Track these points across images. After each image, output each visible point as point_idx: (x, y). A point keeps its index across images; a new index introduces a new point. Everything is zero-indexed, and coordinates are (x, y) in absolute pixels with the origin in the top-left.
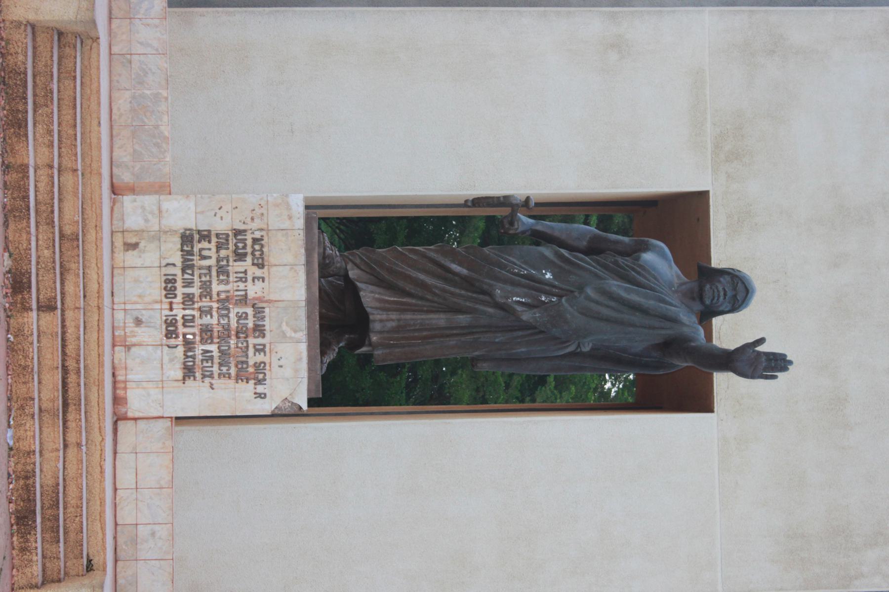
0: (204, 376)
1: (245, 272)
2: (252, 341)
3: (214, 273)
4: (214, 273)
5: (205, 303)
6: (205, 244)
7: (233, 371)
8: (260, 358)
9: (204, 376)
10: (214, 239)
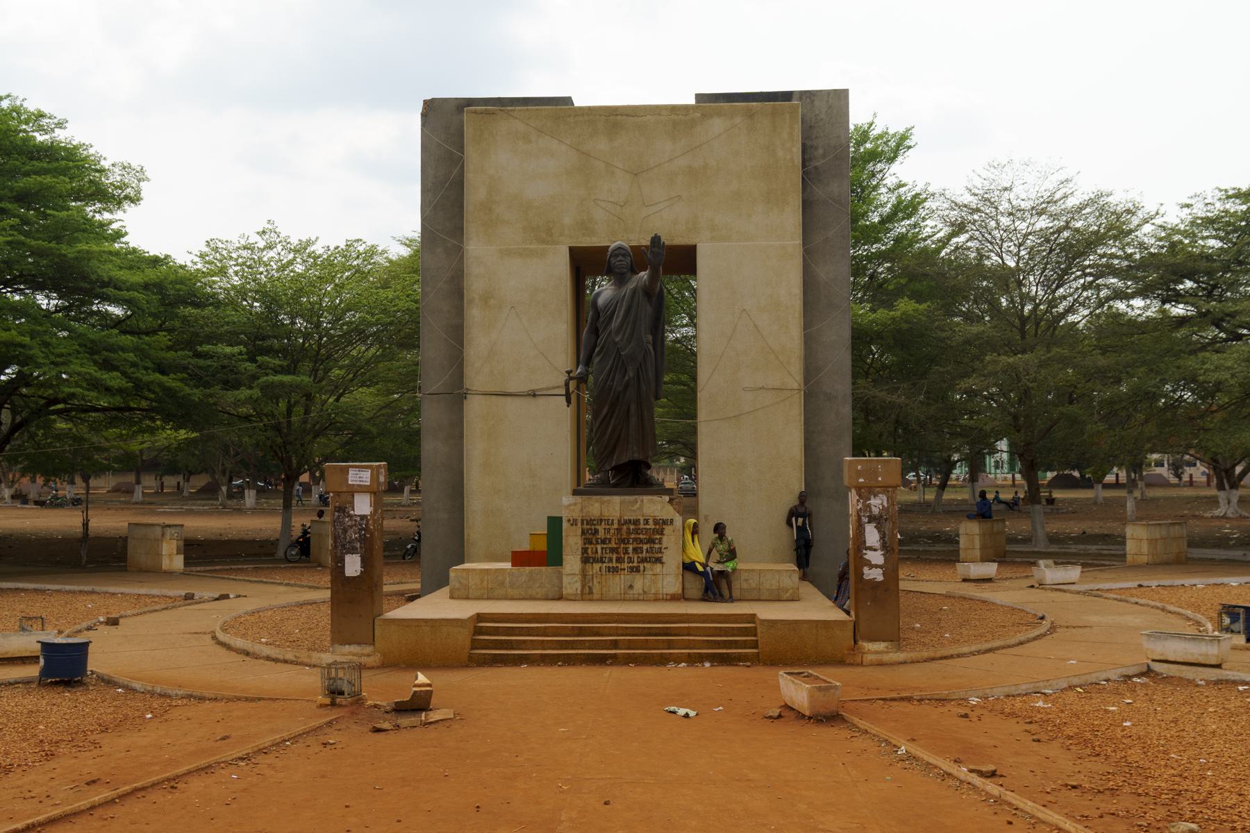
0: (661, 552)
1: (605, 529)
2: (642, 526)
3: (605, 546)
4: (605, 546)
5: (621, 550)
6: (590, 551)
7: (658, 537)
8: (651, 522)
9: (661, 552)
10: (587, 546)
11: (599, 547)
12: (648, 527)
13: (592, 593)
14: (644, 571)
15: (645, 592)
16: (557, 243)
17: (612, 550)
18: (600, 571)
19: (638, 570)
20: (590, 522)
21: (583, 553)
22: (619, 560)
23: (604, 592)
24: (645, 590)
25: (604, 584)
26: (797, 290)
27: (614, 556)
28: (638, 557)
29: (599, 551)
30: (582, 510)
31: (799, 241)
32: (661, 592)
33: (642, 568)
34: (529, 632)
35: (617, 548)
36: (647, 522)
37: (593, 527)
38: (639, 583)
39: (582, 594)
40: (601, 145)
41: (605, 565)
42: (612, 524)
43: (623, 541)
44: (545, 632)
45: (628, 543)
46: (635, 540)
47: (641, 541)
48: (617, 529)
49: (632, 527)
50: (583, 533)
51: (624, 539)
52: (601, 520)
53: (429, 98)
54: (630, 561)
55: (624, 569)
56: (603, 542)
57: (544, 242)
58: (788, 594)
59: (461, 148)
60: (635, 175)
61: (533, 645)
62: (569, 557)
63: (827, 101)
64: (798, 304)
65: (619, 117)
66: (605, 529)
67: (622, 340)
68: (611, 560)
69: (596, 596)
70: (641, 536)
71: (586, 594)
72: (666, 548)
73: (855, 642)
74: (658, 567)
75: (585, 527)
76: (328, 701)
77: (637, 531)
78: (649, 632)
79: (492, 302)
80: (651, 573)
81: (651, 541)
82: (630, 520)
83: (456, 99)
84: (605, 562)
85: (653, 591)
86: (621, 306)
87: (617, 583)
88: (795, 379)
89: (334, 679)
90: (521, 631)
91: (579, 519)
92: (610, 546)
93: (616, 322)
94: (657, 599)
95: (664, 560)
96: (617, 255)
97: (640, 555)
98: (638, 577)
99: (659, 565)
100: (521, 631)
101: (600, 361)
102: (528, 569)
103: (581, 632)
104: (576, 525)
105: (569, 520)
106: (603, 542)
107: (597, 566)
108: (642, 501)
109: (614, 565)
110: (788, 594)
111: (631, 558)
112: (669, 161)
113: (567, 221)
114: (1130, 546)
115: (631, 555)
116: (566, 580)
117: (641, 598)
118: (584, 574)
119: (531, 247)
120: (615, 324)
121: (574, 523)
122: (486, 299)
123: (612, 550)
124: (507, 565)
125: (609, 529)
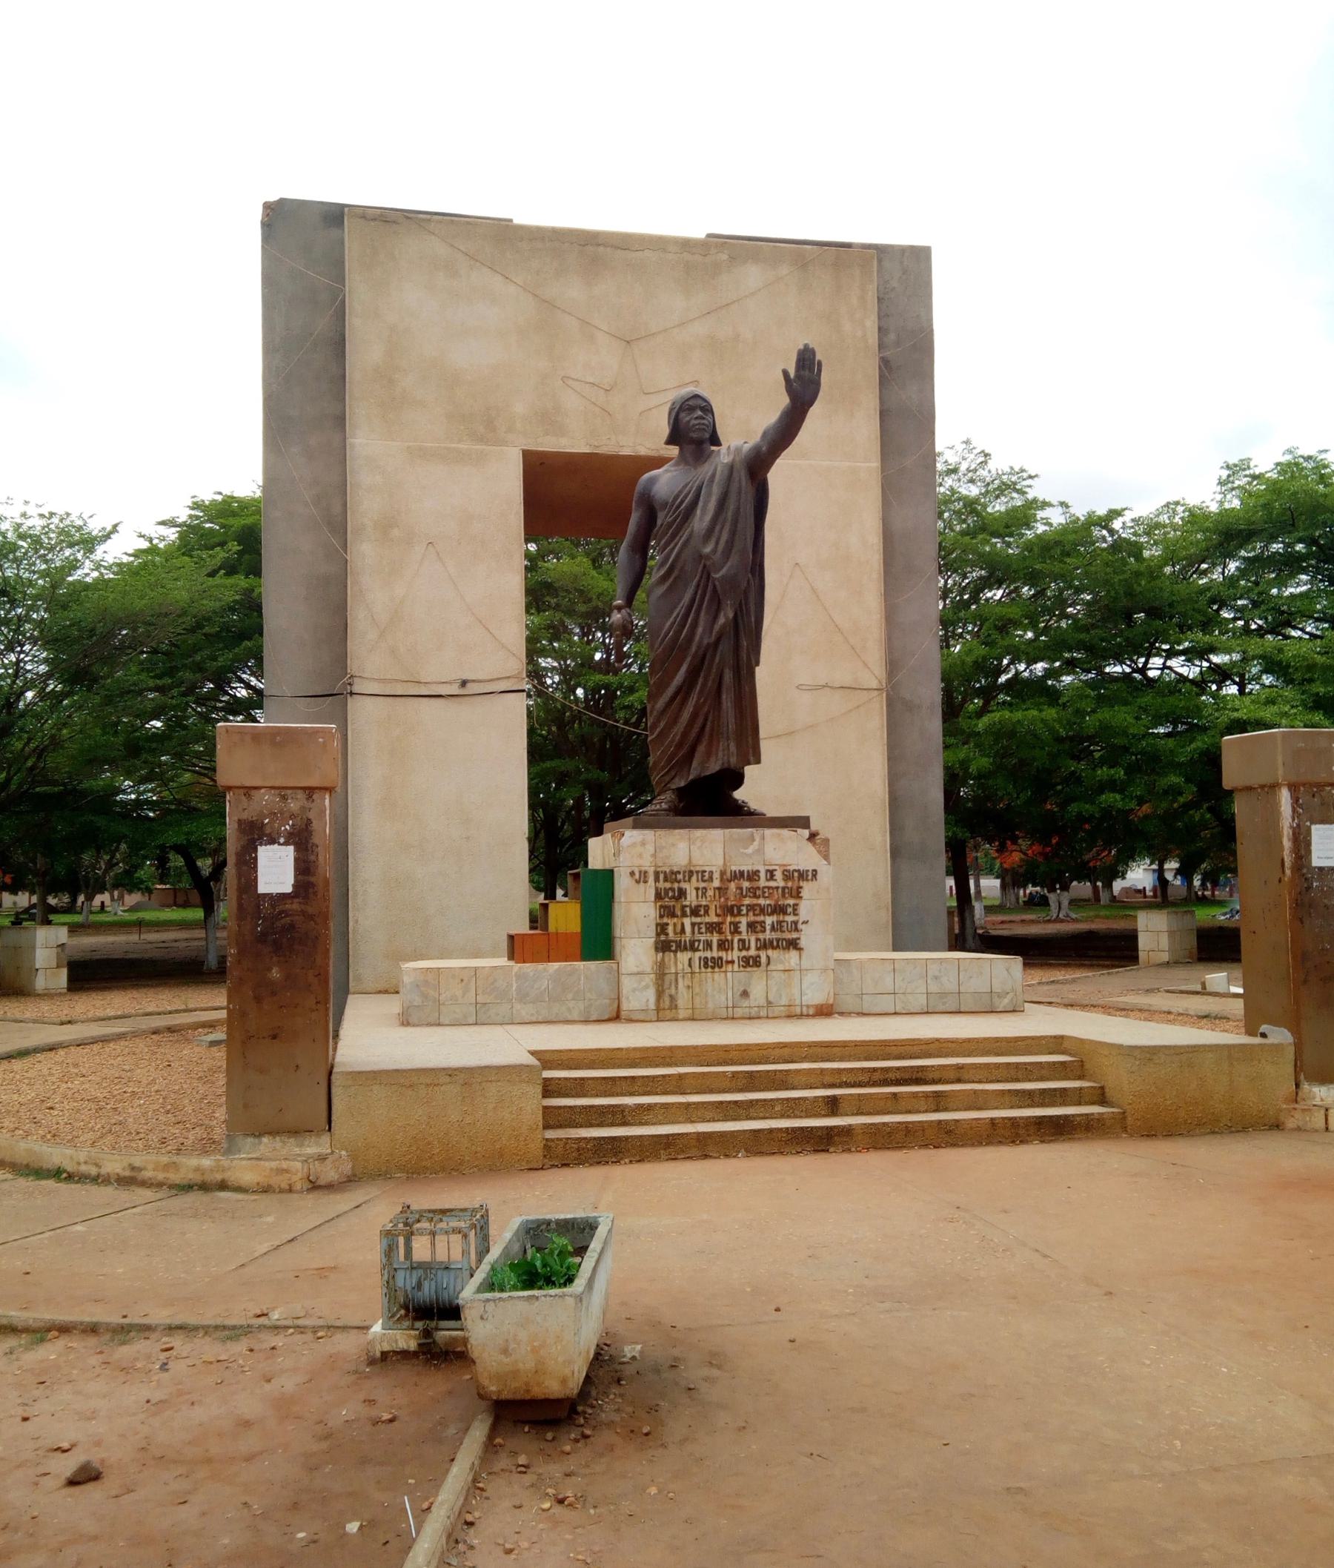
0: (797, 930)
4: (698, 920)
5: (726, 927)
7: (791, 902)
8: (778, 875)
9: (797, 930)
10: (665, 920)
11: (687, 922)
12: (772, 884)
13: (676, 1007)
14: (768, 964)
15: (769, 1003)
16: (503, 443)
17: (712, 928)
18: (690, 965)
19: (756, 962)
20: (671, 876)
21: (658, 935)
22: (723, 945)
23: (697, 1005)
24: (771, 998)
25: (697, 990)
26: (875, 540)
27: (715, 939)
28: (758, 940)
29: (688, 928)
30: (654, 856)
31: (875, 464)
32: (798, 1002)
33: (764, 960)
34: (649, 1085)
35: (719, 924)
36: (771, 875)
37: (676, 885)
38: (759, 985)
39: (658, 1009)
40: (572, 291)
41: (698, 954)
42: (711, 879)
43: (730, 910)
44: (678, 1084)
45: (739, 914)
46: (751, 908)
47: (762, 911)
48: (719, 889)
49: (746, 884)
50: (658, 896)
51: (732, 907)
52: (691, 873)
53: (273, 198)
54: (744, 945)
55: (732, 962)
56: (695, 912)
57: (482, 440)
58: (1006, 1001)
59: (341, 279)
60: (628, 342)
61: (668, 1113)
62: (633, 941)
63: (901, 263)
64: (875, 558)
65: (601, 249)
66: (697, 889)
67: (714, 551)
68: (709, 945)
69: (682, 1014)
70: (762, 901)
71: (665, 1010)
72: (805, 922)
73: (1297, 1085)
74: (792, 957)
75: (662, 885)
76: (406, 1339)
77: (754, 892)
78: (886, 1078)
79: (395, 532)
80: (781, 967)
81: (780, 910)
82: (742, 873)
83: (322, 203)
84: (697, 950)
85: (784, 1001)
86: (709, 494)
87: (720, 987)
88: (873, 672)
89: (421, 1266)
90: (632, 1085)
91: (651, 871)
92: (707, 919)
93: (701, 519)
94: (793, 1015)
95: (802, 943)
96: (692, 409)
97: (761, 936)
98: (757, 974)
99: (793, 954)
100: (632, 1085)
101: (664, 595)
102: (555, 966)
103: (752, 1082)
104: (645, 882)
105: (632, 874)
106: (695, 912)
107: (683, 957)
108: (763, 838)
109: (715, 954)
110: (1006, 1001)
111: (743, 941)
112: (678, 326)
113: (519, 408)
114: (1144, 942)
115: (744, 936)
116: (627, 984)
117: (763, 1013)
118: (661, 973)
119: (461, 446)
120: (701, 521)
121: (641, 878)
122: (386, 526)
123: (712, 928)
124: (503, 961)
125: (705, 888)
